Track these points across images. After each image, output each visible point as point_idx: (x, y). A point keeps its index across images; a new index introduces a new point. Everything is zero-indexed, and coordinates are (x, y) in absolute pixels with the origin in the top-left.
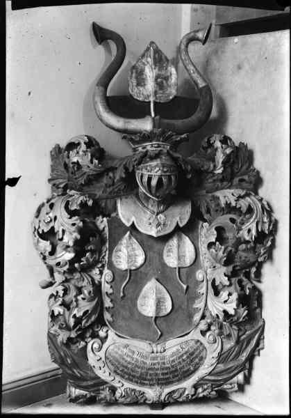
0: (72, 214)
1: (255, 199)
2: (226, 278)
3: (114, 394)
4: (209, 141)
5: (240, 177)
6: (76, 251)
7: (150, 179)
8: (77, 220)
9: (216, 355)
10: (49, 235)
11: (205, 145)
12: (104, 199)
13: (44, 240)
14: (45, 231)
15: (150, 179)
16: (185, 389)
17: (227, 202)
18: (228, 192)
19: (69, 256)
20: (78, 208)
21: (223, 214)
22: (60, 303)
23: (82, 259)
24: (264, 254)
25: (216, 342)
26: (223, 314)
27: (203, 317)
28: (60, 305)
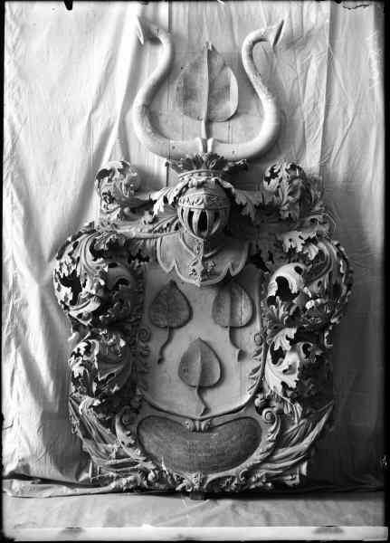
0: (96, 254)
1: (331, 246)
2: (288, 342)
3: (147, 476)
4: (272, 169)
5: (318, 281)
6: (100, 299)
7: (191, 214)
8: (103, 262)
9: (273, 436)
10: (73, 282)
11: (268, 175)
12: (141, 239)
13: (66, 286)
14: (67, 275)
15: (191, 214)
16: (233, 478)
17: (255, 206)
18: (295, 235)
19: (93, 306)
20: (106, 248)
21: (289, 263)
22: (80, 362)
23: (109, 311)
24: (338, 314)
25: (273, 423)
26: (281, 387)
27: (223, 461)
28: (81, 365)
